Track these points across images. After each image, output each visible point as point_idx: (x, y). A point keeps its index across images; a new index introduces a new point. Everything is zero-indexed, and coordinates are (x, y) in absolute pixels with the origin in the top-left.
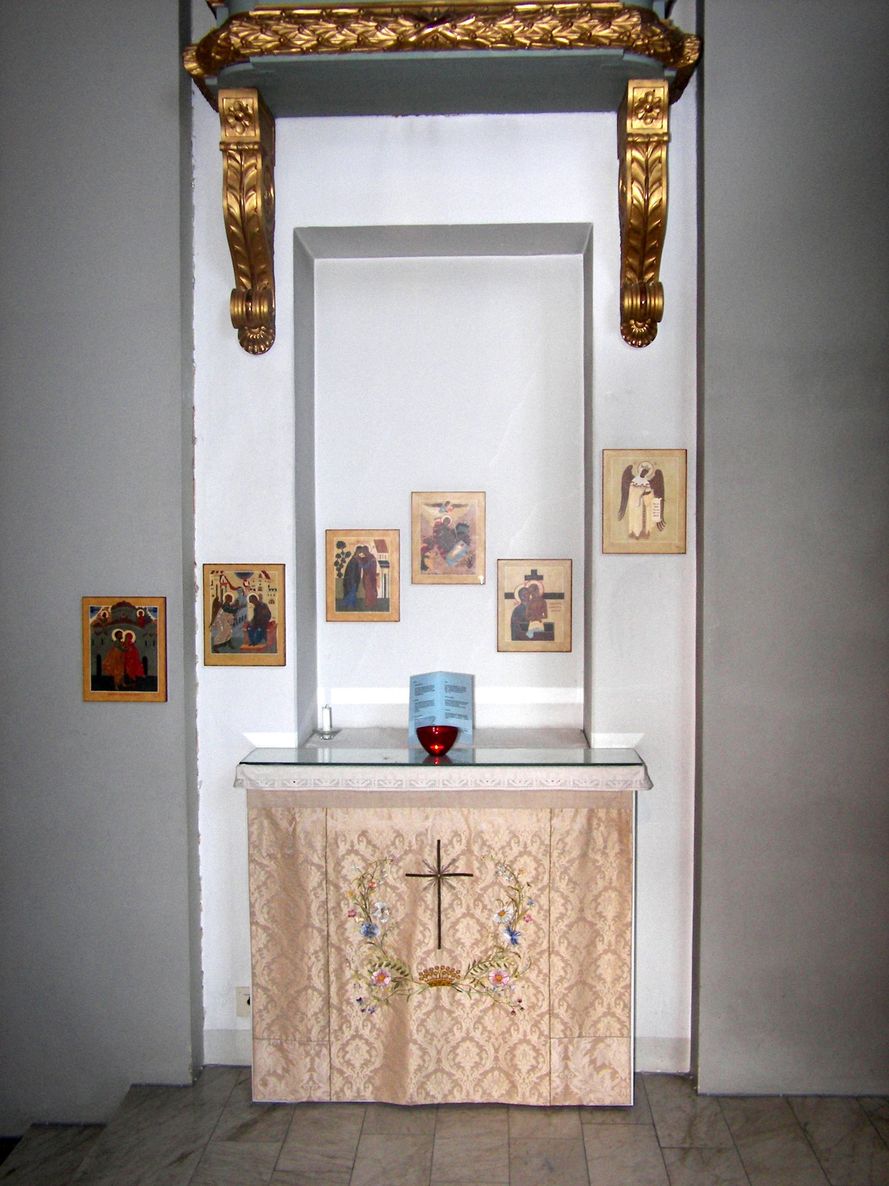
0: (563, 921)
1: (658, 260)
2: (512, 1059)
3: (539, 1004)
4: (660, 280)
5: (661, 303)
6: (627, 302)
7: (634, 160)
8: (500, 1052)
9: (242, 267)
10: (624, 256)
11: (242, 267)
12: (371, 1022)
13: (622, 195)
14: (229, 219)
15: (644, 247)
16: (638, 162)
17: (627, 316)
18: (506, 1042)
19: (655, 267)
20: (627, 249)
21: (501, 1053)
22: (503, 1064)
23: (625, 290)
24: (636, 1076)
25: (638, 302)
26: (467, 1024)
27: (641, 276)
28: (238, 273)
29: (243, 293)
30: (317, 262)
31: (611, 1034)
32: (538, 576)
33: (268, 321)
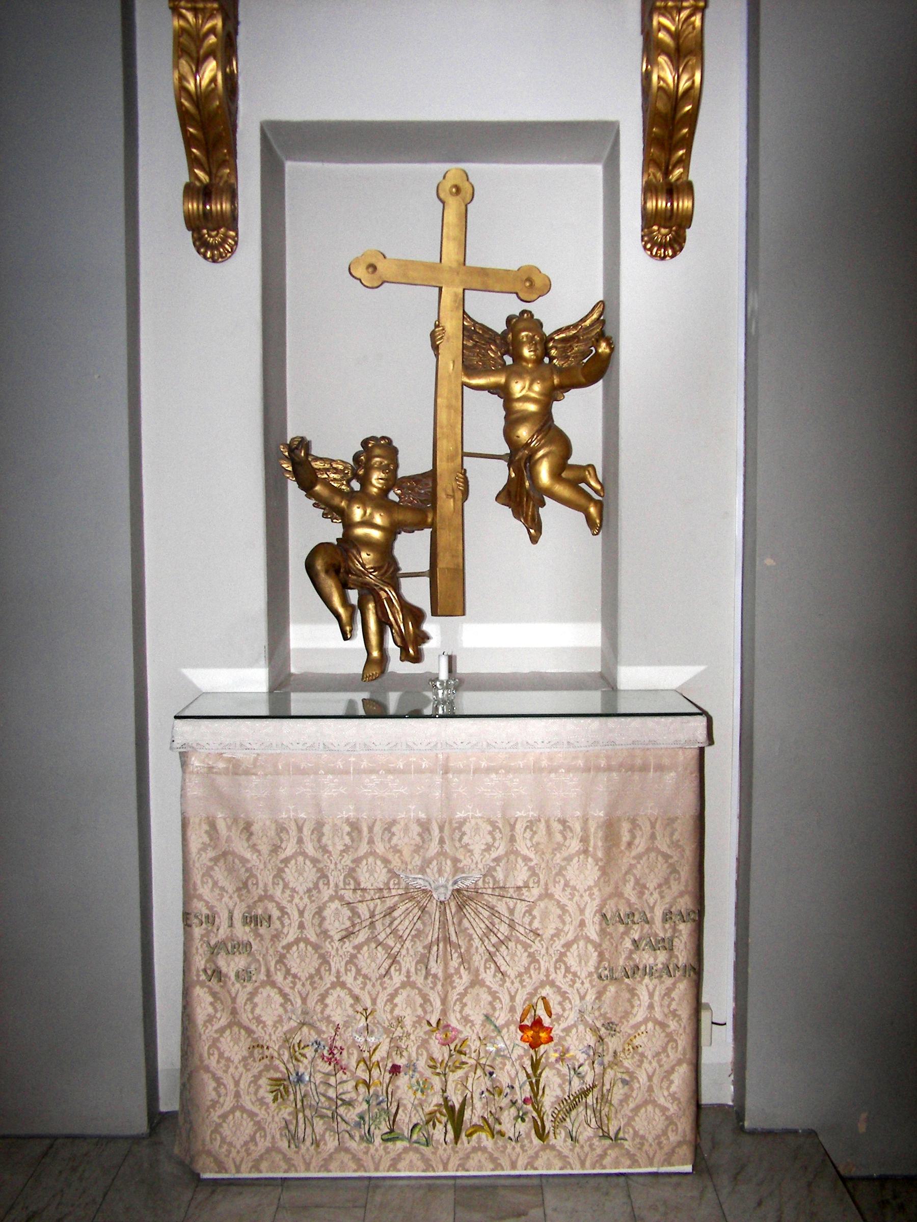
0: (559, 939)
1: (692, 133)
2: (320, 925)
3: (566, 1015)
4: (691, 178)
5: (690, 204)
6: (651, 205)
7: (662, 27)
8: (306, 914)
9: (191, 130)
10: (646, 151)
11: (191, 130)
12: (427, 1050)
13: (646, 77)
14: (182, 89)
15: (671, 136)
16: (667, 30)
17: (649, 219)
18: (315, 988)
19: (685, 162)
20: (649, 140)
21: (308, 915)
22: (310, 849)
23: (649, 190)
24: (705, 1120)
25: (662, 204)
26: (337, 963)
27: (667, 173)
28: (193, 162)
29: (199, 189)
30: (289, 165)
31: (369, 1052)
32: (475, 985)
33: (231, 221)
